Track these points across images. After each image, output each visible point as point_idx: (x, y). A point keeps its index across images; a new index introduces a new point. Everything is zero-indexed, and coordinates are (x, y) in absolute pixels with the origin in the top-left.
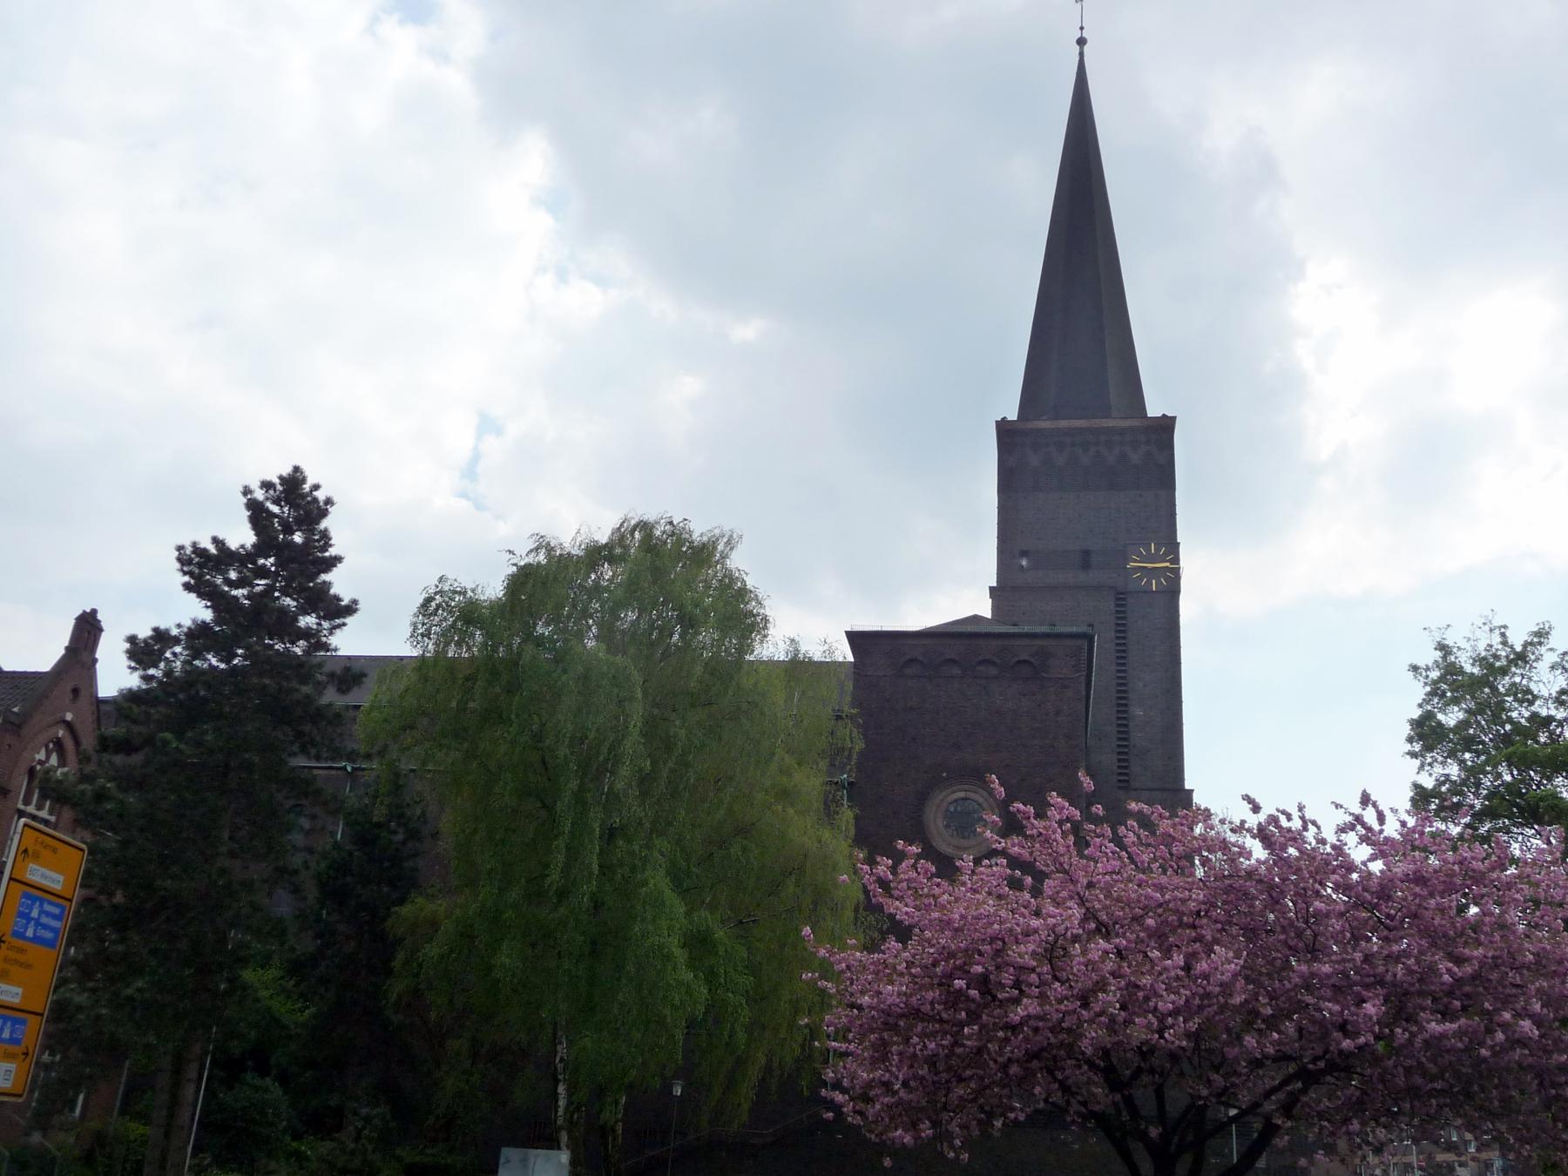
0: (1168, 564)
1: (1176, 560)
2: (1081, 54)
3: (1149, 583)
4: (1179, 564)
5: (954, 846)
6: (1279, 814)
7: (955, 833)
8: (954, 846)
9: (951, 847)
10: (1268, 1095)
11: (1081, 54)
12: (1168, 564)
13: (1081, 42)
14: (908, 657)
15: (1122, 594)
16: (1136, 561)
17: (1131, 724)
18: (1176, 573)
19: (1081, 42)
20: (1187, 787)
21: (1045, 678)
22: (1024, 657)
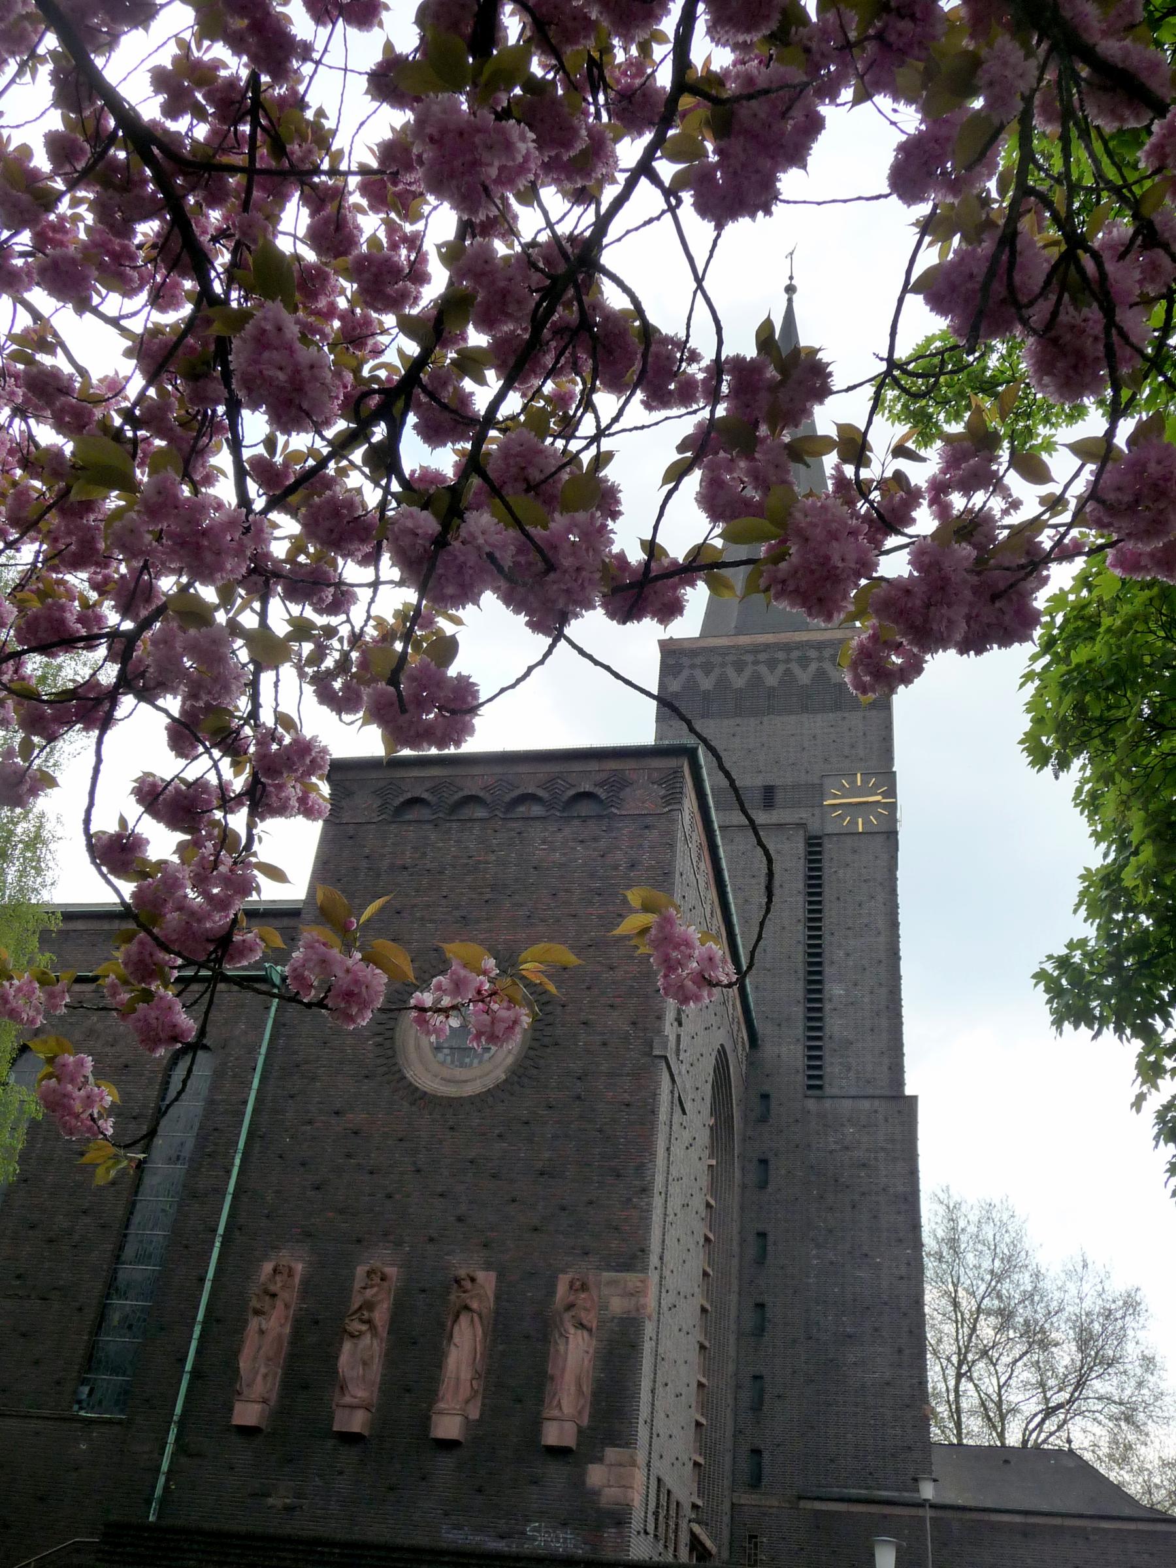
0: (879, 798)
1: (892, 792)
2: (790, 301)
3: (854, 822)
4: (895, 797)
5: (442, 1079)
6: (644, 79)
7: (449, 1059)
8: (442, 1079)
9: (437, 1080)
10: (38, 756)
11: (790, 301)
12: (879, 798)
13: (790, 289)
14: (409, 796)
15: (816, 838)
16: (835, 796)
17: (828, 1007)
18: (892, 807)
19: (790, 289)
20: (909, 1091)
21: (615, 814)
22: (587, 787)
